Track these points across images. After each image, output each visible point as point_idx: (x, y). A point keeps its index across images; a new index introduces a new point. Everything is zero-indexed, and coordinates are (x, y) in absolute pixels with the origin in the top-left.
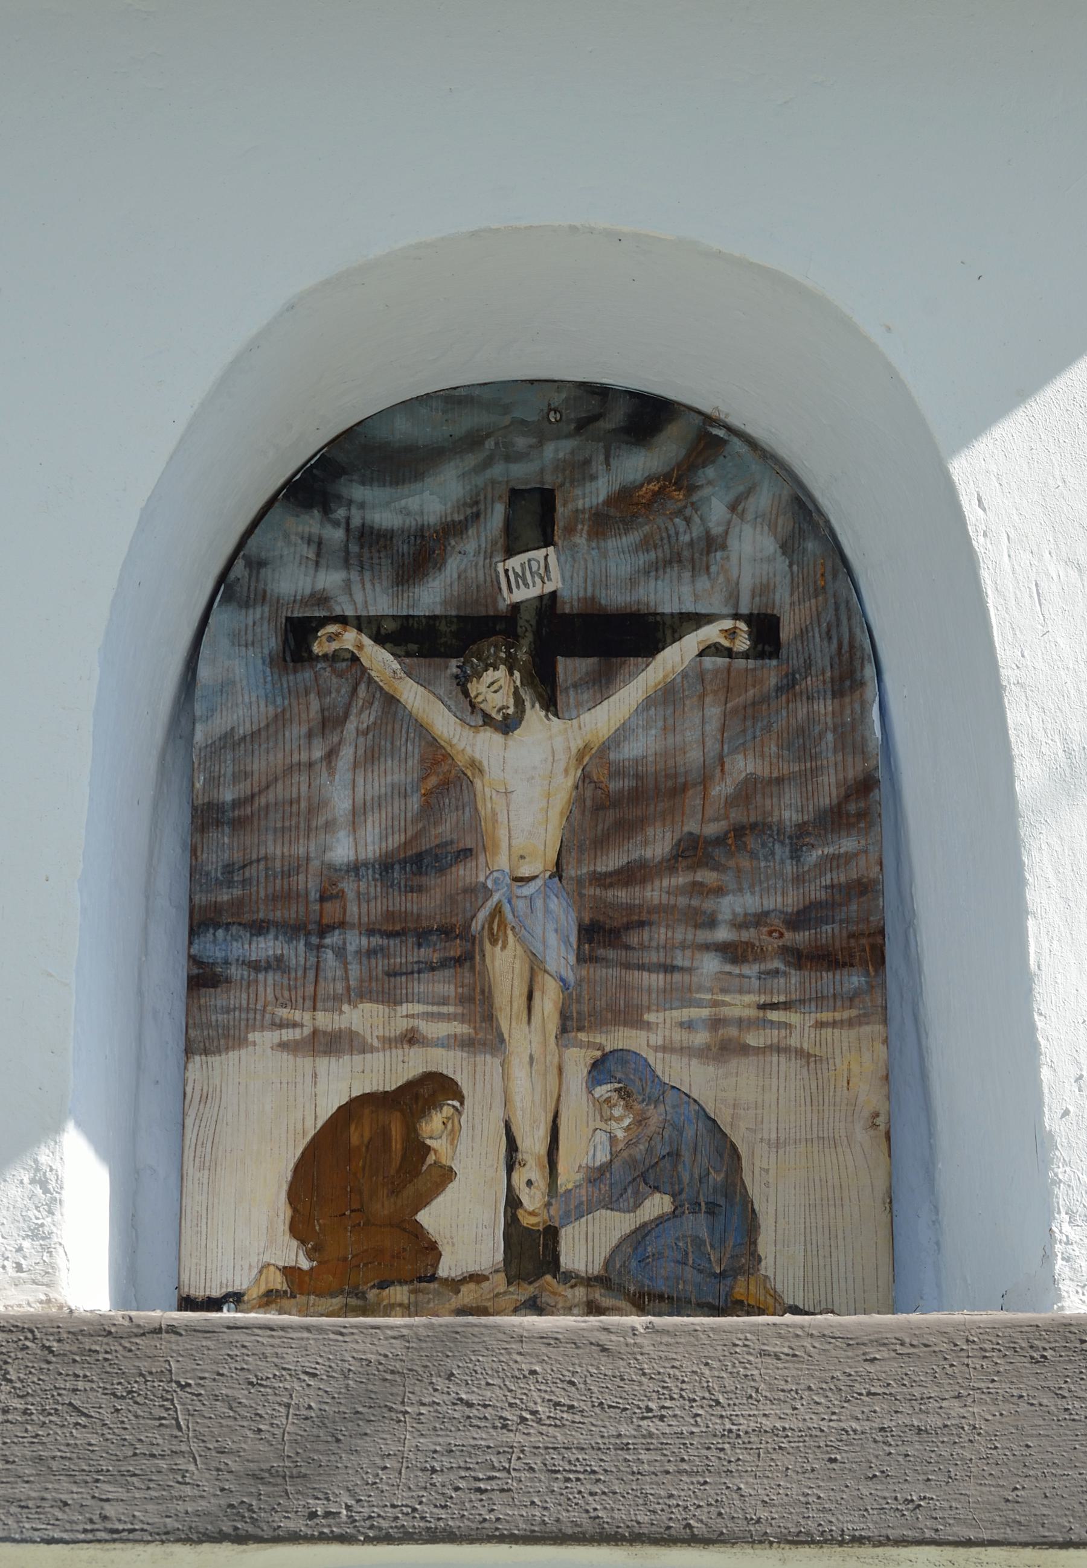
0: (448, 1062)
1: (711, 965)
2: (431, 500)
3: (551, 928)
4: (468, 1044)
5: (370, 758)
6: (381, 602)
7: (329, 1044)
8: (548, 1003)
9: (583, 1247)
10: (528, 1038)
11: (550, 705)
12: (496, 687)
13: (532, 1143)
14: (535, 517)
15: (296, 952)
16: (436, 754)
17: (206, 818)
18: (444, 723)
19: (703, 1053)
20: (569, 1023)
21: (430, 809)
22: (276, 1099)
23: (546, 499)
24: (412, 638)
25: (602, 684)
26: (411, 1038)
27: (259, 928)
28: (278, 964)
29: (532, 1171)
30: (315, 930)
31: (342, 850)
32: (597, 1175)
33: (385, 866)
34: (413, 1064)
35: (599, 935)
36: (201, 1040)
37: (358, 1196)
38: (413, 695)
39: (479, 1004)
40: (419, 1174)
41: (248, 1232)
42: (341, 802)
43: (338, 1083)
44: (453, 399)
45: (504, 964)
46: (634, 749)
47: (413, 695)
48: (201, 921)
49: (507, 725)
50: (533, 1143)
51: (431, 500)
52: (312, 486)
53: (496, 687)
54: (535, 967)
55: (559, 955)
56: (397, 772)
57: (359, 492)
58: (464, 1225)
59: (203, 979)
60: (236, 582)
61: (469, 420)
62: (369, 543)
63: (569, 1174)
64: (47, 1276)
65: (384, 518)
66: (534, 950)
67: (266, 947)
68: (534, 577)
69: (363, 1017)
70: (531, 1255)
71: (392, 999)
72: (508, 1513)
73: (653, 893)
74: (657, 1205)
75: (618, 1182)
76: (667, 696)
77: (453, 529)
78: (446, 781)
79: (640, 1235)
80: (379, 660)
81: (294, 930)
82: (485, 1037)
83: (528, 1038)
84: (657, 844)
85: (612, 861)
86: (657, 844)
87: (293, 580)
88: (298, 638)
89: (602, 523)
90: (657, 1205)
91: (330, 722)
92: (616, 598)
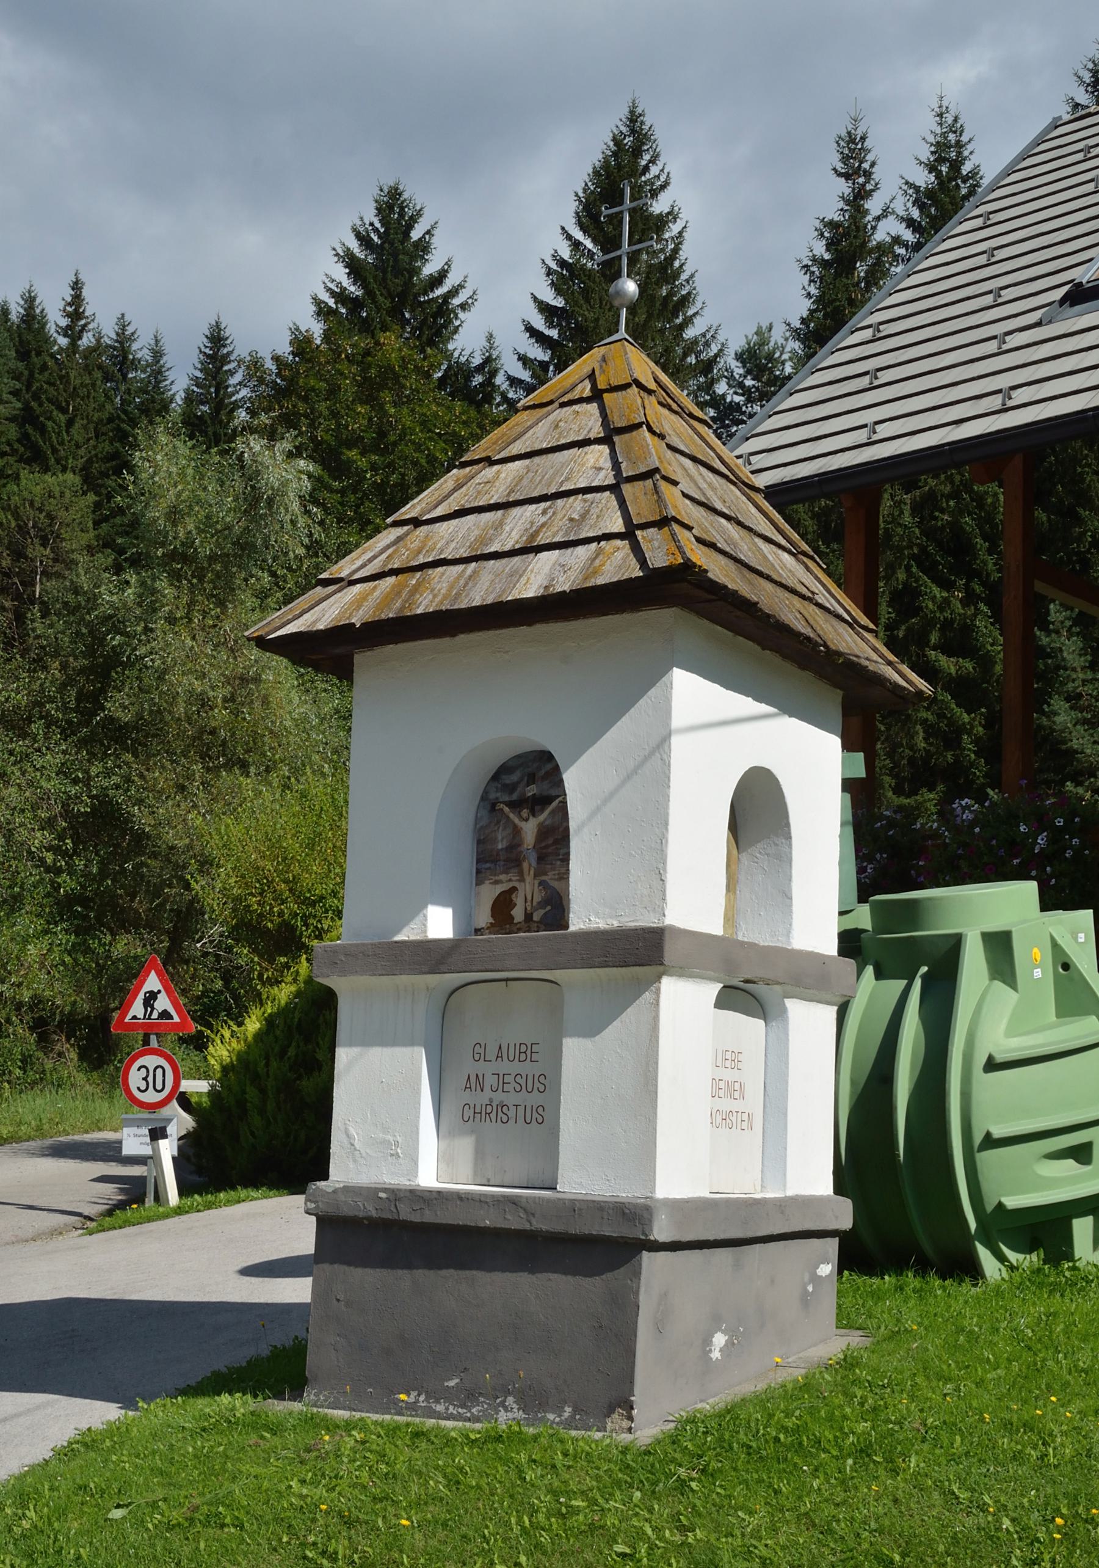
0: (516, 884)
1: (559, 863)
2: (514, 777)
3: (533, 858)
4: (519, 881)
5: (504, 829)
6: (507, 799)
7: (497, 882)
8: (532, 872)
9: (536, 917)
10: (529, 879)
11: (534, 816)
12: (525, 813)
13: (529, 898)
14: (532, 779)
15: (492, 866)
16: (515, 826)
17: (479, 842)
18: (517, 821)
19: (557, 880)
20: (535, 876)
21: (514, 837)
22: (489, 893)
23: (534, 775)
24: (512, 805)
25: (542, 811)
26: (510, 880)
27: (487, 862)
28: (489, 868)
29: (529, 903)
30: (495, 861)
31: (500, 847)
32: (539, 903)
33: (507, 848)
34: (511, 885)
35: (541, 859)
36: (479, 883)
37: (502, 907)
38: (511, 816)
39: (521, 874)
40: (512, 905)
41: (484, 918)
42: (500, 838)
43: (499, 889)
44: (519, 756)
45: (525, 865)
46: (547, 823)
47: (511, 816)
48: (478, 861)
49: (527, 820)
50: (529, 898)
51: (514, 777)
52: (496, 777)
53: (525, 813)
54: (530, 865)
55: (534, 864)
56: (509, 831)
57: (504, 777)
58: (518, 914)
59: (478, 872)
60: (484, 798)
61: (503, 770)
62: (505, 786)
63: (535, 903)
64: (425, 932)
65: (508, 782)
66: (530, 863)
67: (488, 865)
68: (532, 790)
69: (503, 877)
70: (528, 917)
71: (507, 873)
72: (474, 968)
73: (549, 850)
74: (549, 908)
75: (542, 904)
76: (553, 812)
77: (518, 783)
78: (517, 831)
79: (545, 914)
80: (506, 809)
81: (492, 862)
82: (522, 880)
83: (529, 879)
84: (550, 841)
85: (543, 844)
86: (550, 841)
87: (492, 796)
88: (493, 806)
89: (543, 778)
90: (549, 908)
91: (498, 822)
92: (545, 793)
